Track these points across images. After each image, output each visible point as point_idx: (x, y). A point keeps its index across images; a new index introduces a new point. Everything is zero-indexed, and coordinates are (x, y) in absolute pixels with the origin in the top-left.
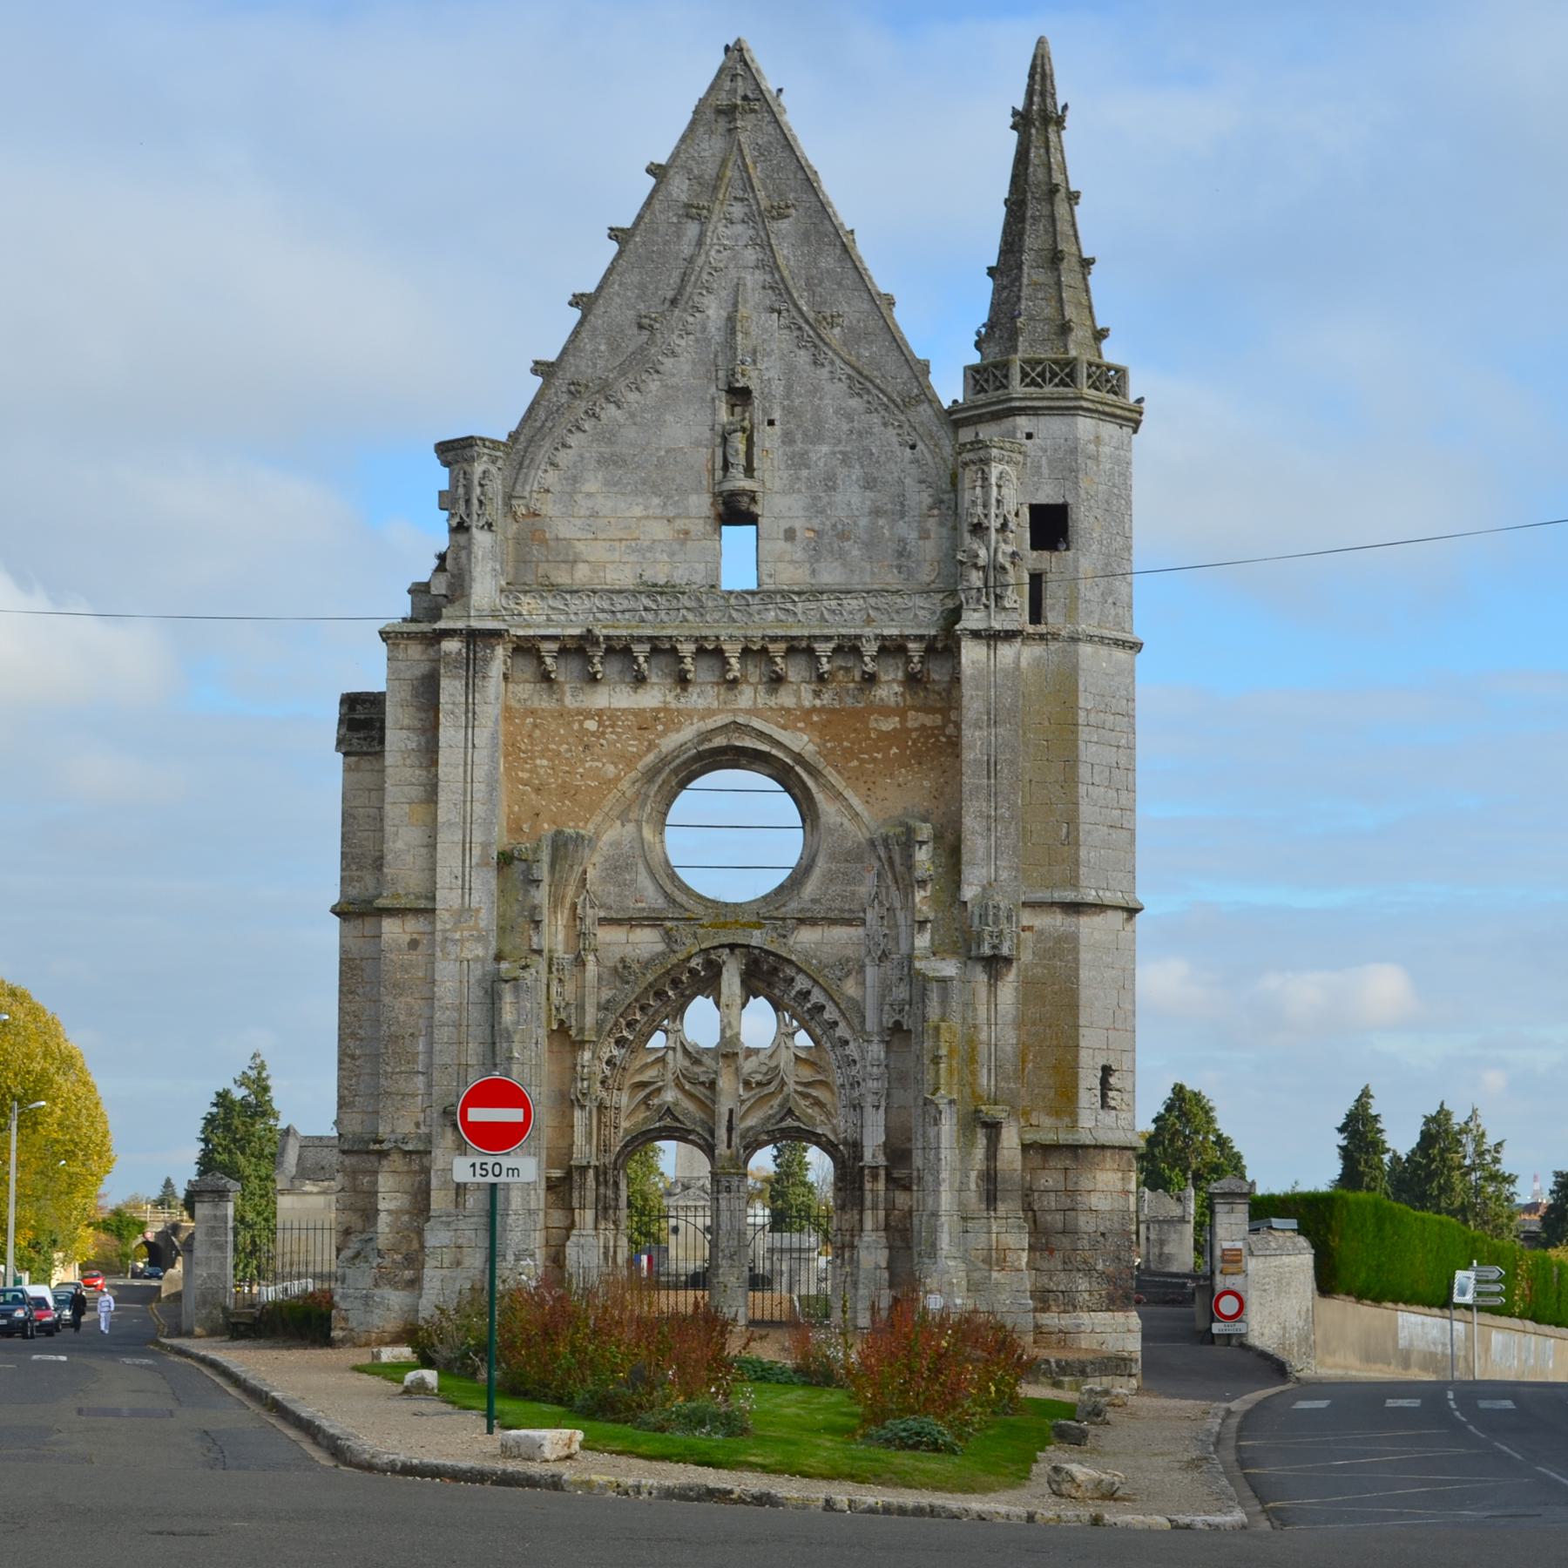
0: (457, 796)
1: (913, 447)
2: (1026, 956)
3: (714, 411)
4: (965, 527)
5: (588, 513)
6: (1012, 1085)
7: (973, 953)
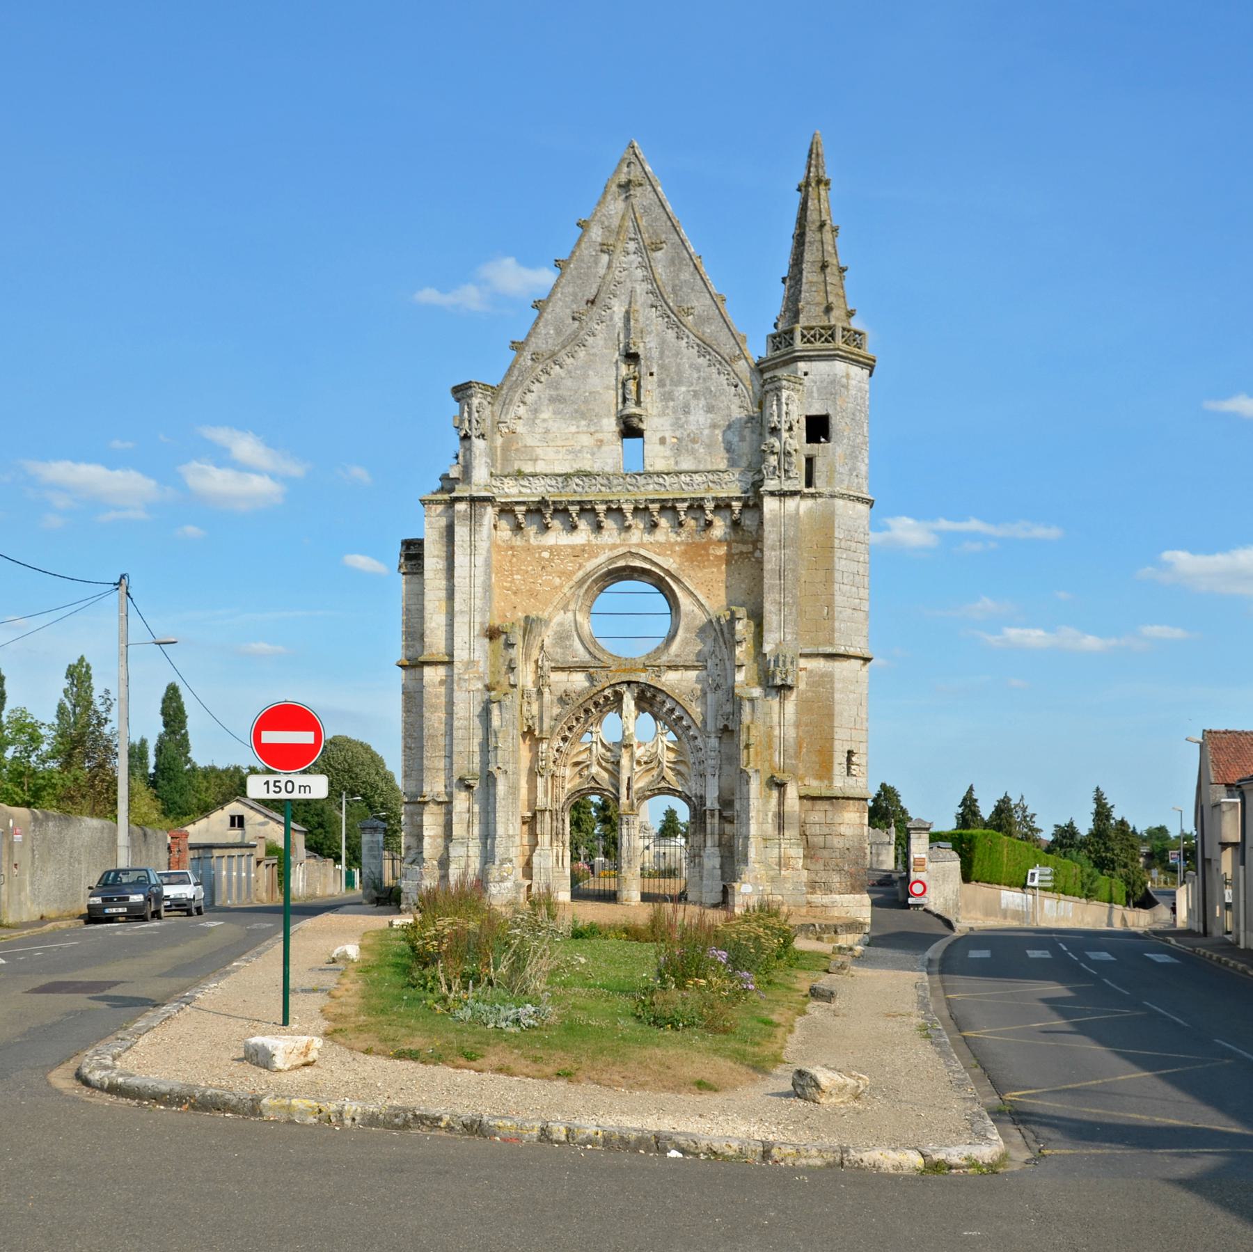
0: (464, 596)
1: (736, 386)
2: (802, 686)
3: (617, 368)
4: (767, 430)
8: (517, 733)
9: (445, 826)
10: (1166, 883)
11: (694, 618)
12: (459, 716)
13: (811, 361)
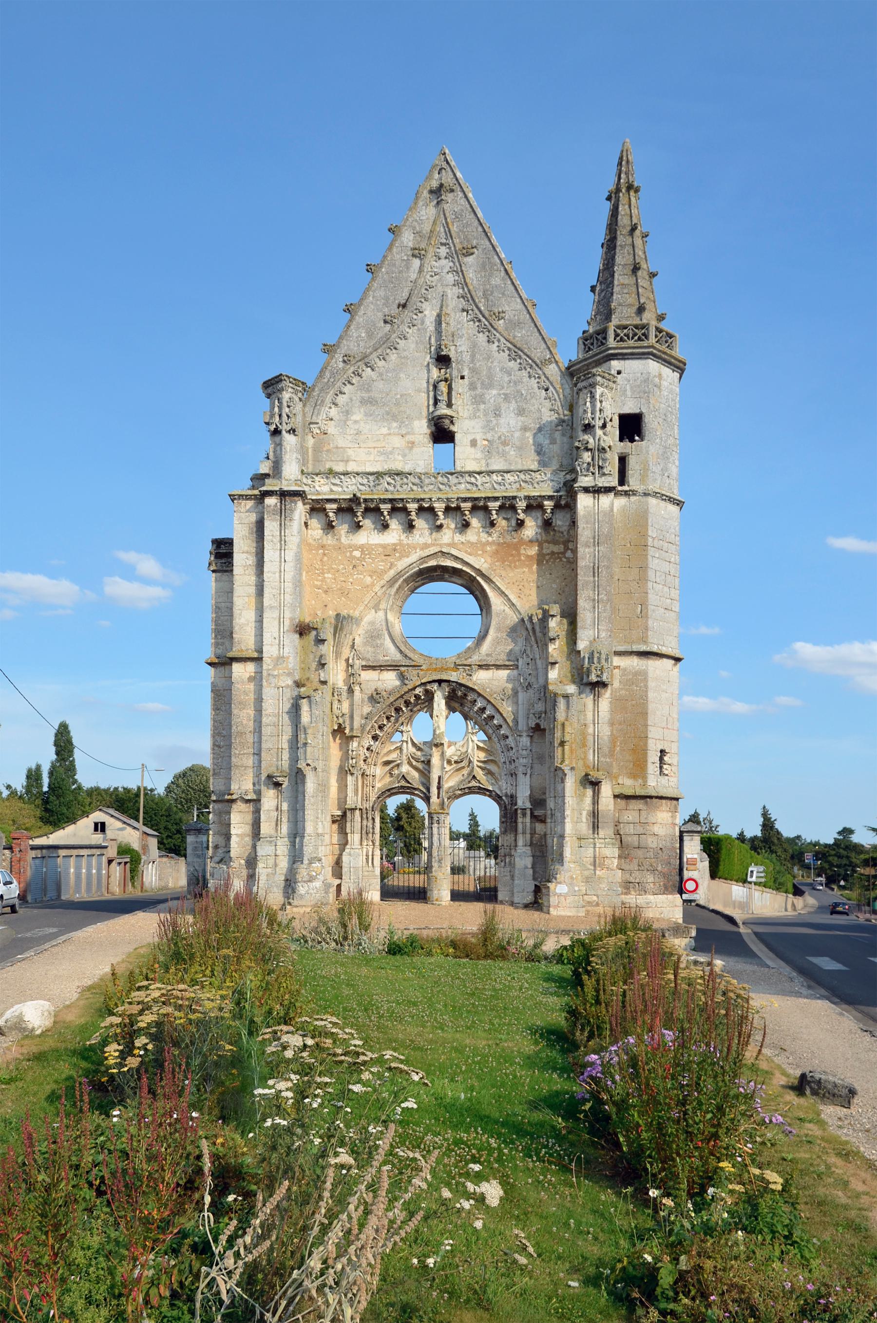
0: (274, 591)
1: (547, 390)
2: (616, 684)
3: (429, 371)
4: (580, 428)
5: (355, 432)
6: (608, 760)
7: (585, 681)
8: (328, 731)
9: (253, 825)
10: (803, 876)
11: (505, 618)
12: (267, 712)
13: (625, 359)
